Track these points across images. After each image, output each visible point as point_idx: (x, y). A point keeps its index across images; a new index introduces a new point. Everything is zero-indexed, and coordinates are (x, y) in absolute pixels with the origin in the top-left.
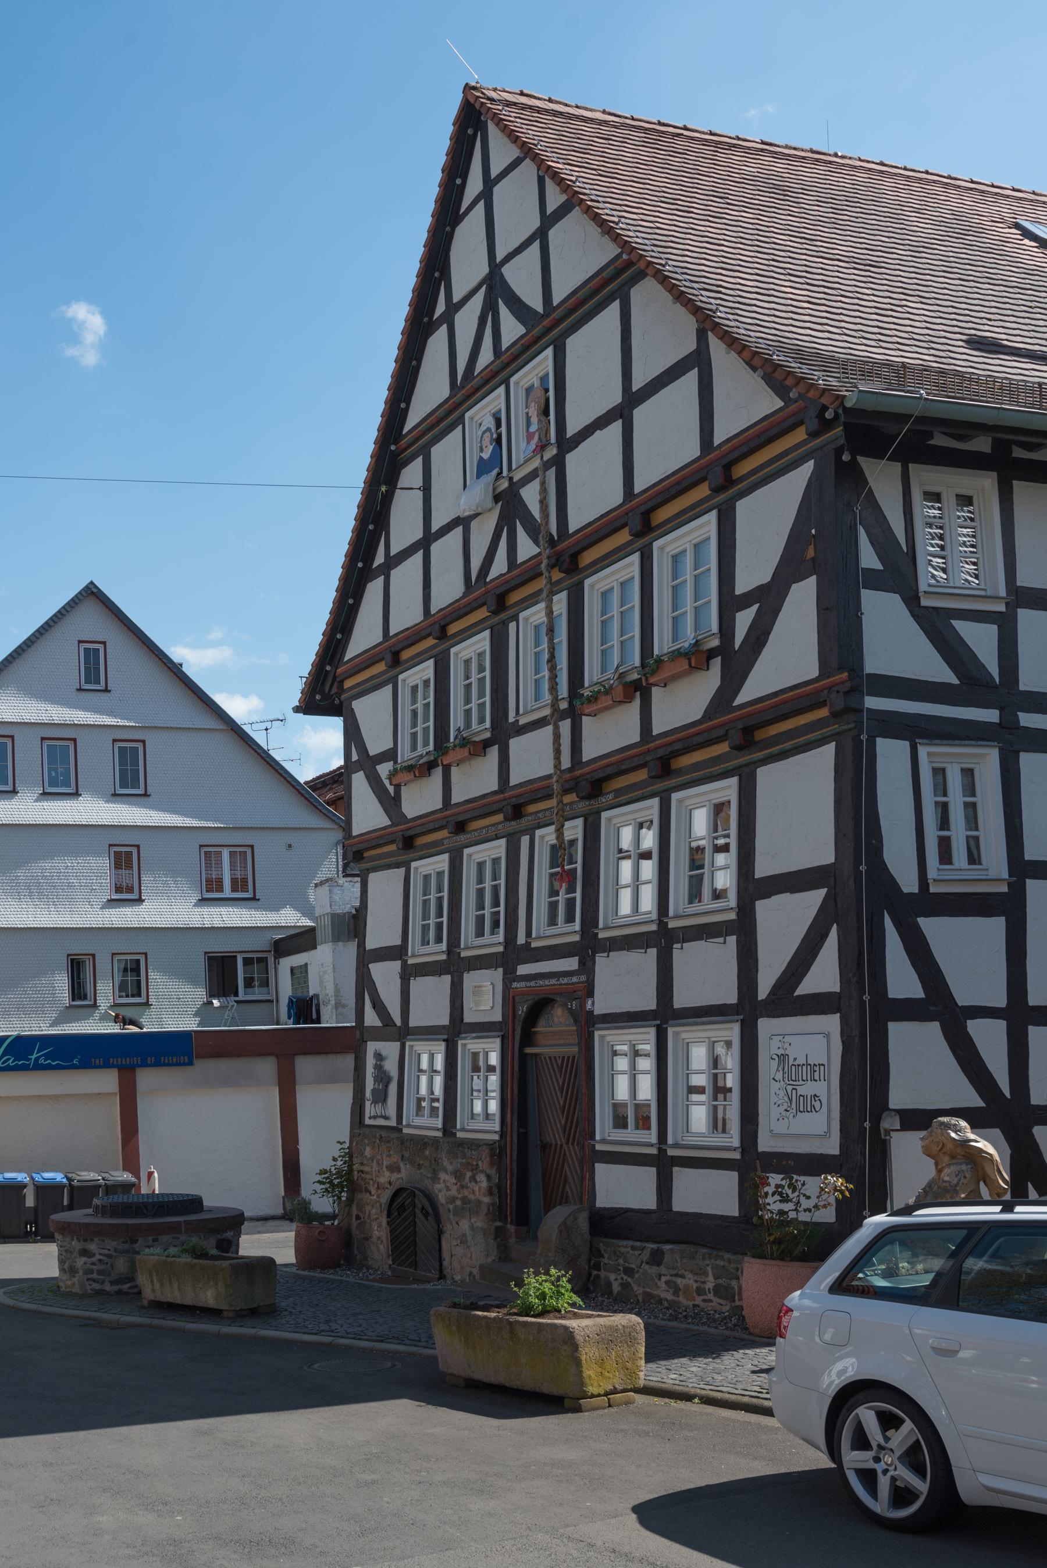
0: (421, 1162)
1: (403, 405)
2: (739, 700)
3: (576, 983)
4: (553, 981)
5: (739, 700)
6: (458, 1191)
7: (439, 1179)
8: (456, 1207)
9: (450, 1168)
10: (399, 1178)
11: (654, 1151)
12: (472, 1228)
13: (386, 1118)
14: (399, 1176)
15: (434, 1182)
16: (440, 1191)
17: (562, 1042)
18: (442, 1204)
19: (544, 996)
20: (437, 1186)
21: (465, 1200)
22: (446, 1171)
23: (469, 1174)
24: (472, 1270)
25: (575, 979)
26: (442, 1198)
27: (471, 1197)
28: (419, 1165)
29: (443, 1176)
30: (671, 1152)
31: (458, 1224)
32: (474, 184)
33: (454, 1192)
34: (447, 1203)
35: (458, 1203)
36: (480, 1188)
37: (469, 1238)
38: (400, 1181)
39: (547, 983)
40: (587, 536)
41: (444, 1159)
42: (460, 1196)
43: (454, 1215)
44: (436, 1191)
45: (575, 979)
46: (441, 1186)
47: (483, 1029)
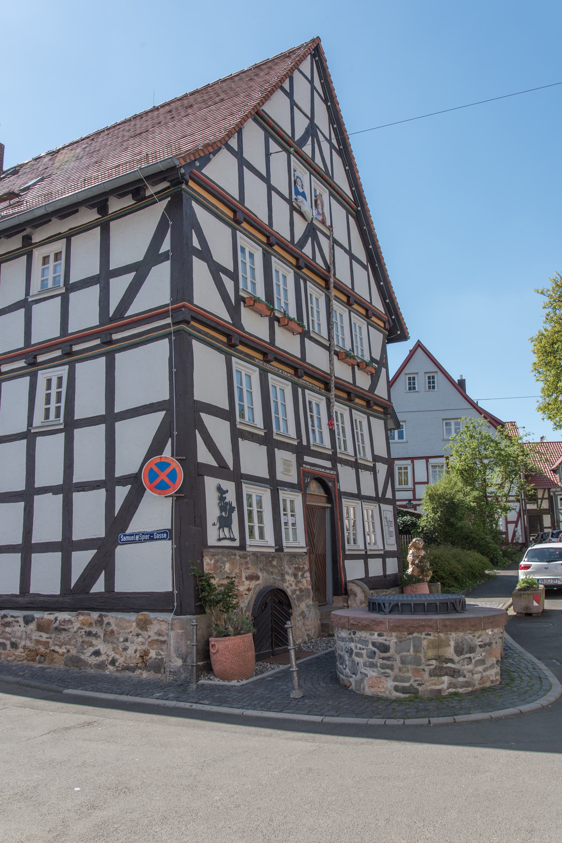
0: (272, 570)
1: (347, 168)
2: (128, 313)
3: (332, 474)
4: (323, 470)
5: (128, 313)
6: (296, 585)
7: (286, 580)
8: (297, 595)
9: (290, 571)
10: (258, 584)
11: (364, 553)
12: (308, 606)
13: (233, 540)
14: (258, 582)
15: (283, 582)
16: (288, 587)
17: (315, 501)
18: (290, 596)
19: (320, 476)
20: (286, 585)
21: (301, 590)
22: (288, 574)
23: (300, 574)
24: (309, 633)
25: (328, 472)
26: (289, 593)
27: (303, 588)
28: (271, 572)
29: (287, 577)
30: (369, 553)
31: (299, 606)
32: (317, 84)
33: (294, 587)
34: (292, 595)
35: (298, 592)
36: (307, 581)
37: (307, 613)
38: (259, 586)
39: (320, 470)
40: (344, 289)
41: (286, 566)
42: (297, 588)
43: (297, 601)
44: (286, 588)
45: (328, 472)
46: (287, 584)
47: (540, 499)
